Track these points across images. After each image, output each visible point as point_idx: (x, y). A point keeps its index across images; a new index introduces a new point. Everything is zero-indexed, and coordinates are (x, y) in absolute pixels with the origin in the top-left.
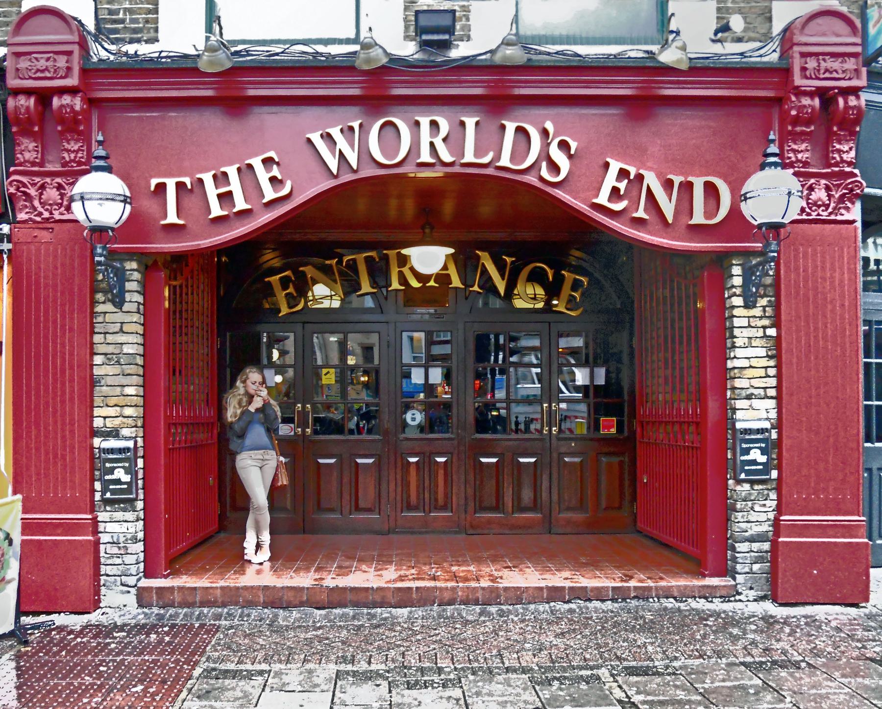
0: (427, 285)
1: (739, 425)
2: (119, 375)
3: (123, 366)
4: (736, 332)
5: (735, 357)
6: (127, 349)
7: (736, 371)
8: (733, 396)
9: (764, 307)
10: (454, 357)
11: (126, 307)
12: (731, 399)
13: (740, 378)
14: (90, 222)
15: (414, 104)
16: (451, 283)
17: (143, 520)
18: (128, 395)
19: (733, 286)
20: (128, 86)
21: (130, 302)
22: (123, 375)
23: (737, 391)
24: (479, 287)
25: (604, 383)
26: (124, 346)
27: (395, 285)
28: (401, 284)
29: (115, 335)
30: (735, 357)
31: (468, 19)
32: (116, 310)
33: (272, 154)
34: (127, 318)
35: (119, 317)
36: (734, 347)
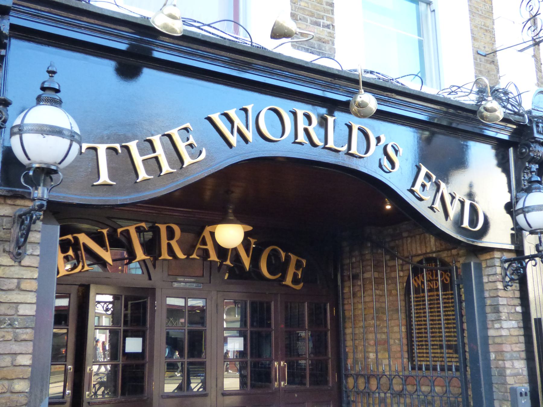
0: (191, 257)
1: (224, 389)
2: (11, 340)
3: (18, 330)
4: (501, 309)
5: (501, 328)
6: (24, 310)
7: (503, 338)
8: (500, 358)
9: (513, 290)
10: (52, 328)
11: (26, 261)
12: (495, 360)
13: (505, 343)
14: (29, 159)
15: (29, 40)
16: (209, 257)
17: (510, 401)
18: (20, 365)
19: (495, 274)
20: (214, 60)
21: (31, 255)
22: (15, 341)
23: (506, 354)
24: (231, 262)
25: (243, 350)
26: (21, 306)
27: (165, 255)
28: (169, 255)
29: (9, 292)
30: (501, 328)
31: (333, 44)
32: (12, 263)
33: (187, 125)
34: (27, 274)
35: (16, 271)
36: (499, 320)
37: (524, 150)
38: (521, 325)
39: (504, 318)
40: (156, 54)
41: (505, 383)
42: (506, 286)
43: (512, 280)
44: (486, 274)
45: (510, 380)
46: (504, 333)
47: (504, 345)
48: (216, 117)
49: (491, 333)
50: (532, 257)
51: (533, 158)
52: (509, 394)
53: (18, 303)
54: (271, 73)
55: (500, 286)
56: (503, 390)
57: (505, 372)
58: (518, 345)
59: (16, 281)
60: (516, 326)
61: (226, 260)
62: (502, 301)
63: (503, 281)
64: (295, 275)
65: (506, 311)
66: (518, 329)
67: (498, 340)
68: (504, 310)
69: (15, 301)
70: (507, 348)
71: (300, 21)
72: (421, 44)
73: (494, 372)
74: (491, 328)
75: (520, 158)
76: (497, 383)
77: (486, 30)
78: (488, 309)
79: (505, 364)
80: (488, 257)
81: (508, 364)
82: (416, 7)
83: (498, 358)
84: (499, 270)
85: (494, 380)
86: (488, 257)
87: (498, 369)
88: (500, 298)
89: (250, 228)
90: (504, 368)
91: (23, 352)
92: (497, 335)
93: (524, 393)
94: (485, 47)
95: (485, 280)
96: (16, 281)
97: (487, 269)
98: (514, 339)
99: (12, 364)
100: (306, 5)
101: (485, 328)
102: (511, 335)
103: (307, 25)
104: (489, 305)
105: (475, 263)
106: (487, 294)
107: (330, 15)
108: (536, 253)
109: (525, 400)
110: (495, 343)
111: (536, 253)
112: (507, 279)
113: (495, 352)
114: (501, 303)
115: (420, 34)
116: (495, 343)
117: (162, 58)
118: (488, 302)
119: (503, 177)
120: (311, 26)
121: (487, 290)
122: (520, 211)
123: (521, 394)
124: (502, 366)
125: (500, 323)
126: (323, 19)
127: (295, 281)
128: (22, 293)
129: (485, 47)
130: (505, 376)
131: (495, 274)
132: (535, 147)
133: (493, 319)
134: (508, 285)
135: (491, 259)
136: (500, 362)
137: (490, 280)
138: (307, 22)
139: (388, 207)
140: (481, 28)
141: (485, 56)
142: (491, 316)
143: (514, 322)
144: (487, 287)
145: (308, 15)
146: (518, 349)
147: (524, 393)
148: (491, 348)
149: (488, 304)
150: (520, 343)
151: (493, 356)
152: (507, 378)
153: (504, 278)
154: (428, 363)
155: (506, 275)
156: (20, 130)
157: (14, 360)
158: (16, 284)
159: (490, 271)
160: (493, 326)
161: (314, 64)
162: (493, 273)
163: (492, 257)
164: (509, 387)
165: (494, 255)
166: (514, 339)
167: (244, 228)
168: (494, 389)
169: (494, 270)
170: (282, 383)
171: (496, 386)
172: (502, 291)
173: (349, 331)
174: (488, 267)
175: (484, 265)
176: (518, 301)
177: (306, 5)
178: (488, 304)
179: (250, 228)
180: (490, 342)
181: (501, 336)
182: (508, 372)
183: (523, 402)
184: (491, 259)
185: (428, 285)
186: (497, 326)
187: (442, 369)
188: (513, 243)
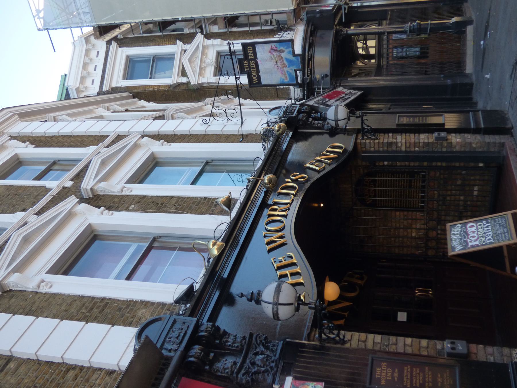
3: (390, 343)
8: (418, 144)
9: (380, 136)
12: (419, 148)
18: (412, 343)
19: (370, 143)
30: (401, 142)
37: (301, 123)
38: (399, 134)
39: (395, 141)
40: (225, 276)
41: (432, 143)
42: (377, 139)
43: (374, 135)
44: (369, 148)
45: (431, 140)
46: (404, 141)
47: (411, 142)
48: (268, 247)
49: (403, 149)
50: (363, 122)
51: (306, 119)
52: (439, 142)
53: (374, 342)
54: (241, 229)
55: (377, 141)
56: (436, 145)
57: (426, 142)
58: (411, 136)
59: (360, 343)
60: (400, 136)
61: (345, 315)
62: (386, 140)
63: (374, 140)
64: (357, 278)
65: (391, 140)
66: (402, 136)
67: (408, 145)
68: (391, 140)
69: (372, 343)
70: (412, 141)
71: (214, 212)
72: (182, 249)
73: (426, 149)
74: (401, 149)
75: (306, 125)
76: (433, 149)
77: (228, 137)
78: (390, 149)
79: (421, 142)
80: (360, 146)
81: (422, 141)
82: (154, 249)
83: (418, 146)
84: (368, 141)
85: (430, 150)
86: (360, 146)
87: (425, 147)
88: (384, 141)
89: (327, 278)
90: (424, 143)
91: (404, 341)
92: (405, 145)
93: (438, 134)
94: (238, 139)
95: (372, 149)
96: (360, 343)
97: (367, 147)
98: (408, 137)
99: (410, 346)
100: (204, 209)
101: (401, 152)
102: (406, 138)
103: (216, 209)
104: (388, 148)
105: (363, 153)
106: (381, 149)
107: (212, 199)
108: (360, 118)
109: (459, 345)
110: (410, 147)
111: (360, 118)
112: (373, 137)
113: (415, 148)
114: (387, 141)
115: (174, 249)
116: (410, 147)
117: (255, 214)
118: (385, 148)
119: (315, 138)
120: (217, 207)
121: (379, 149)
122: (337, 123)
123: (453, 349)
124: (422, 144)
125: (398, 142)
126: (213, 202)
127: (361, 278)
128: (367, 340)
129: (238, 139)
130: (429, 142)
131: (370, 143)
132: (300, 117)
133: (395, 147)
134: (377, 137)
135: (361, 144)
136: (421, 145)
137: (373, 146)
138: (214, 209)
139: (322, 205)
140: (226, 139)
141: (243, 139)
142: (394, 148)
143: (398, 137)
144: (377, 149)
145: (210, 209)
146: (413, 137)
147: (438, 134)
148: (412, 149)
149: (387, 149)
150: (410, 135)
151: (417, 149)
152: (429, 142)
153: (372, 139)
154: (420, 201)
155: (371, 138)
156: (337, 121)
157: (408, 345)
158: (362, 343)
159: (368, 146)
160: (399, 147)
161: (243, 202)
162: (369, 144)
163: (360, 144)
164: (434, 141)
165: (358, 143)
166: (408, 137)
167: (327, 282)
168: (436, 150)
169: (367, 143)
170: (430, 293)
171: (434, 149)
172: (380, 140)
173: (397, 251)
174: (365, 147)
175: (364, 149)
176: (386, 135)
177: (204, 209)
178: (387, 149)
179: (327, 278)
180: (408, 150)
181: (406, 143)
182: (426, 141)
183: (461, 348)
184: (361, 144)
185: (372, 187)
186: (399, 145)
187: (423, 202)
188: (352, 135)
